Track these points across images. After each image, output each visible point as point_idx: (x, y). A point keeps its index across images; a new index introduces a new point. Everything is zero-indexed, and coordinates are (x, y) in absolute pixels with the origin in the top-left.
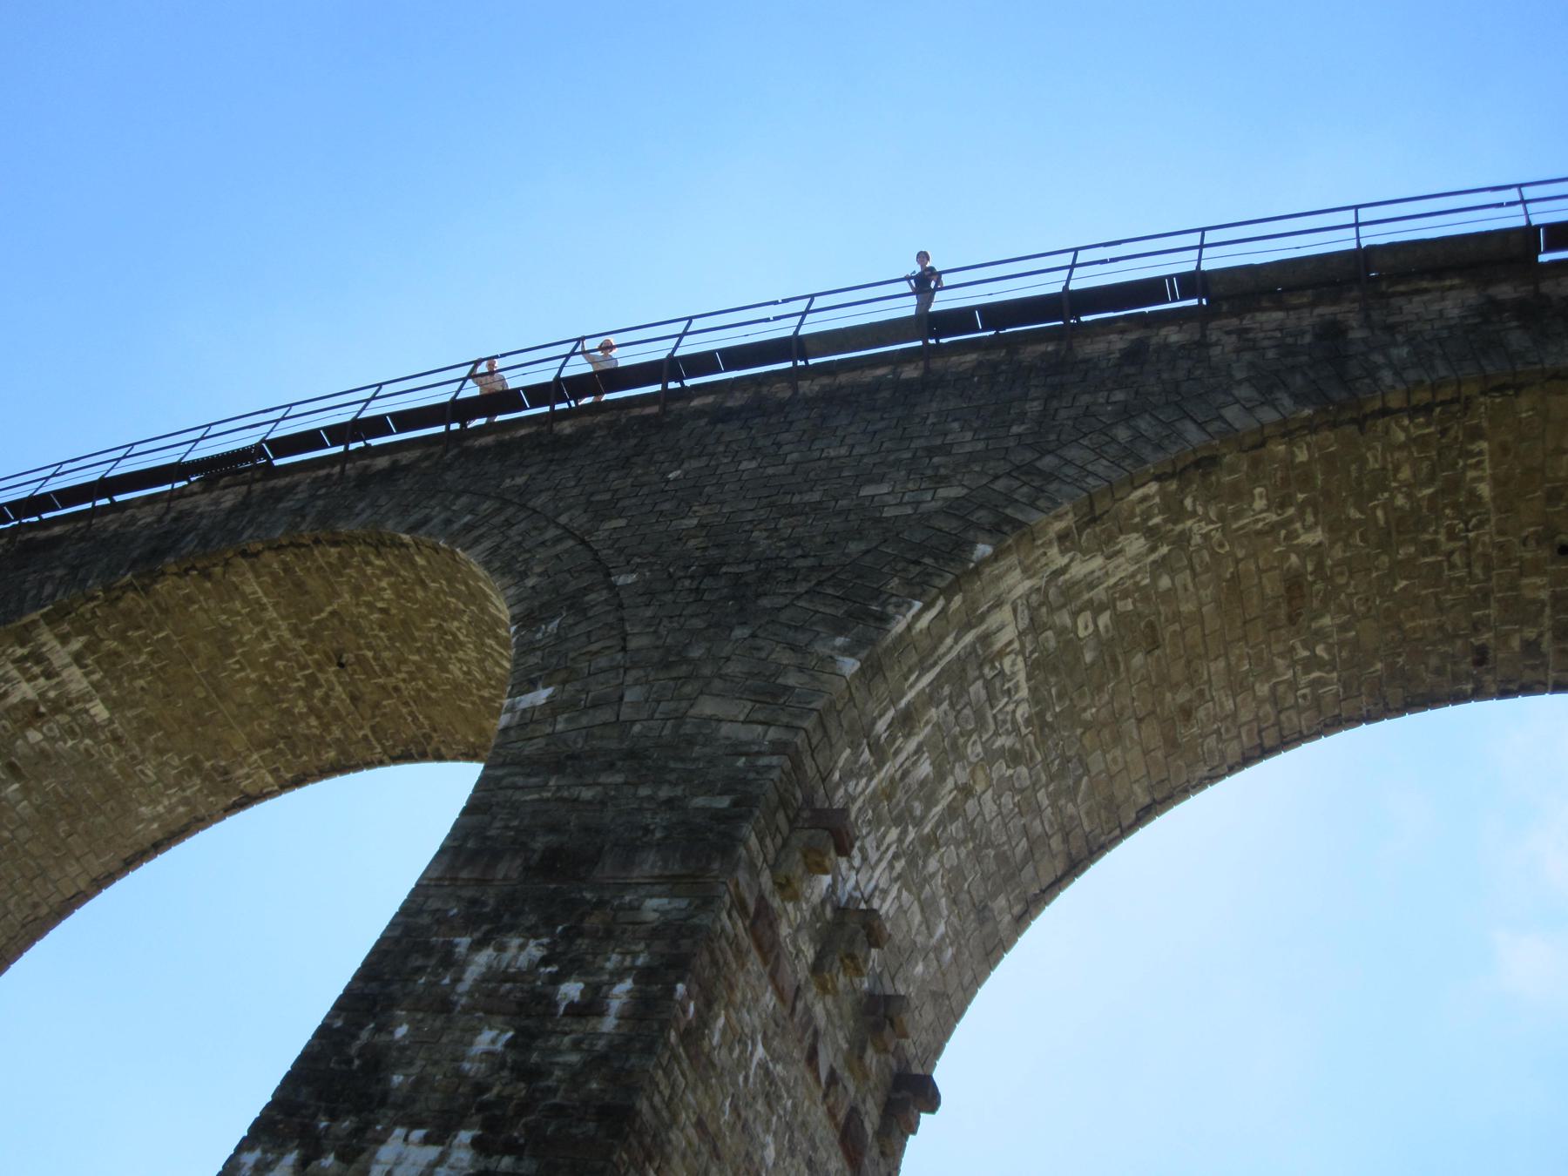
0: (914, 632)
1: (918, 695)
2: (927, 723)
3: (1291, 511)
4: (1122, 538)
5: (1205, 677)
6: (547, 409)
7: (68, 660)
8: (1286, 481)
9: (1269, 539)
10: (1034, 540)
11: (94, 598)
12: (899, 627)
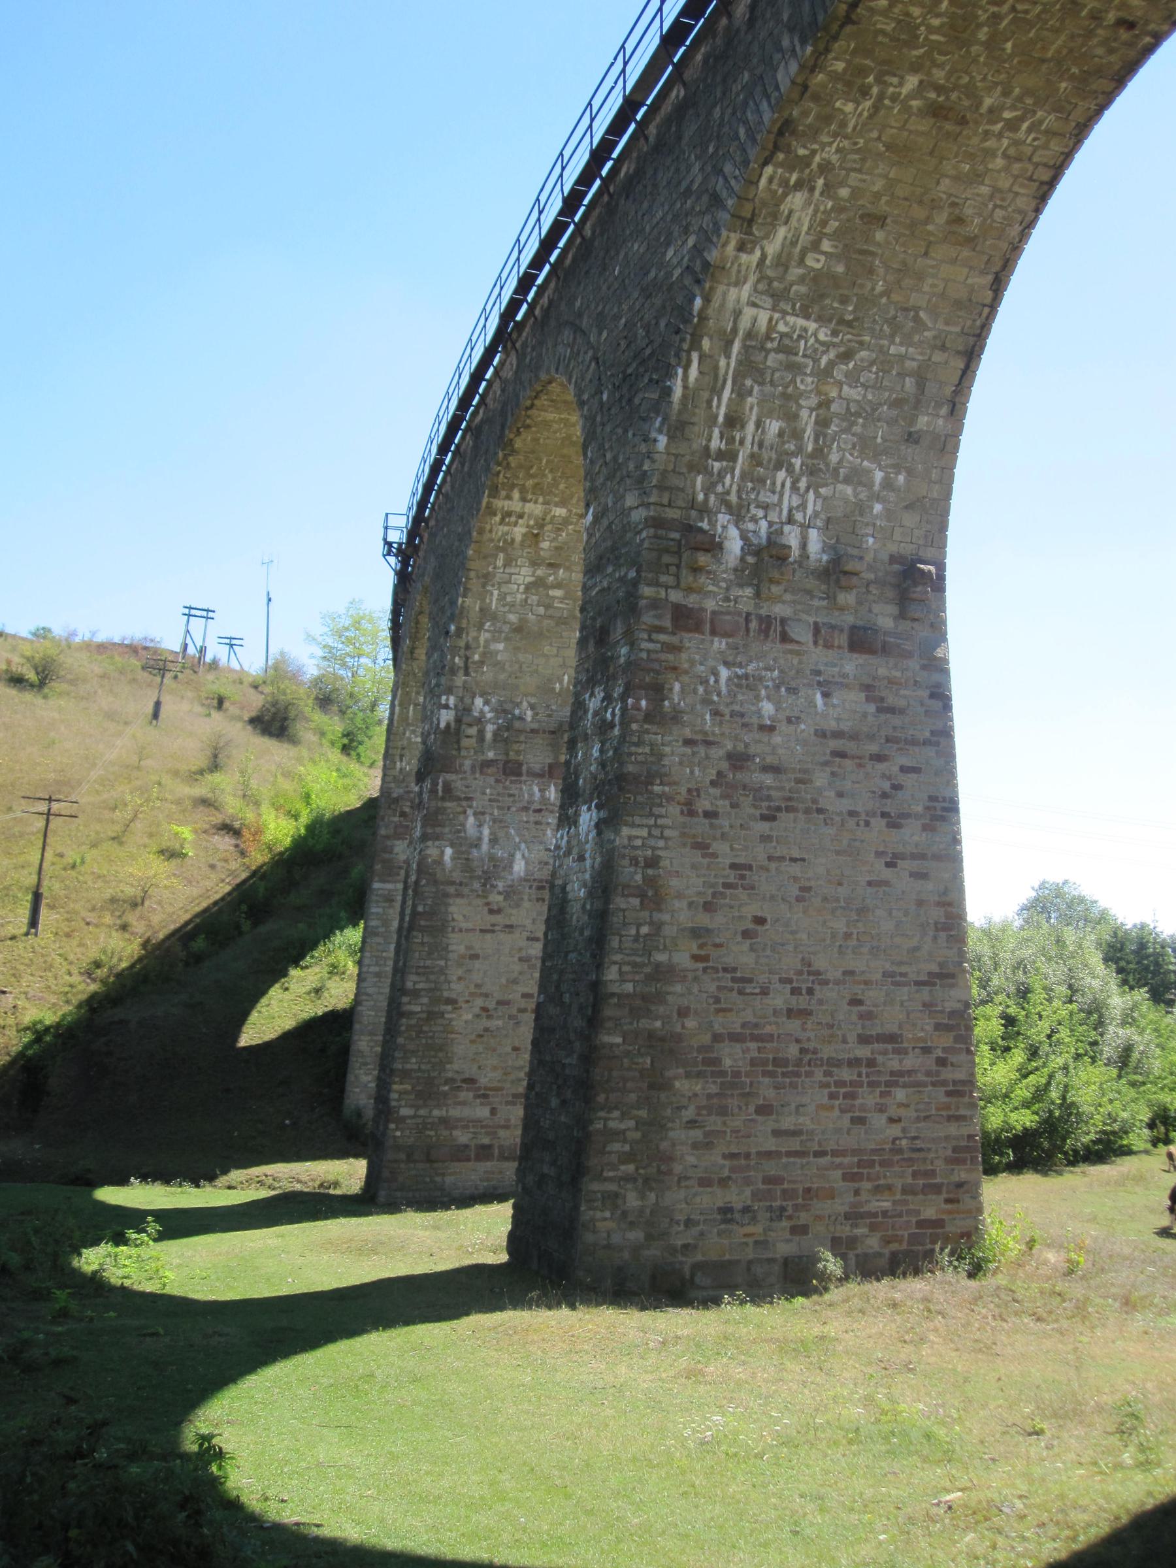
0: (691, 386)
1: (728, 406)
2: (751, 409)
3: (875, 90)
4: (782, 207)
5: (944, 196)
6: (633, 126)
7: (521, 504)
8: (849, 84)
9: (882, 112)
10: (723, 268)
11: (499, 473)
12: (678, 392)
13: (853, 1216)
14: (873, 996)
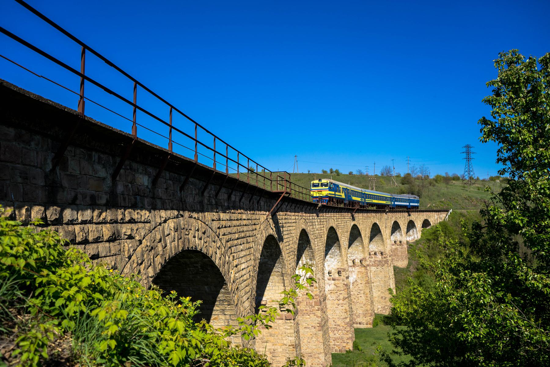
13: (334, 345)
14: (336, 320)
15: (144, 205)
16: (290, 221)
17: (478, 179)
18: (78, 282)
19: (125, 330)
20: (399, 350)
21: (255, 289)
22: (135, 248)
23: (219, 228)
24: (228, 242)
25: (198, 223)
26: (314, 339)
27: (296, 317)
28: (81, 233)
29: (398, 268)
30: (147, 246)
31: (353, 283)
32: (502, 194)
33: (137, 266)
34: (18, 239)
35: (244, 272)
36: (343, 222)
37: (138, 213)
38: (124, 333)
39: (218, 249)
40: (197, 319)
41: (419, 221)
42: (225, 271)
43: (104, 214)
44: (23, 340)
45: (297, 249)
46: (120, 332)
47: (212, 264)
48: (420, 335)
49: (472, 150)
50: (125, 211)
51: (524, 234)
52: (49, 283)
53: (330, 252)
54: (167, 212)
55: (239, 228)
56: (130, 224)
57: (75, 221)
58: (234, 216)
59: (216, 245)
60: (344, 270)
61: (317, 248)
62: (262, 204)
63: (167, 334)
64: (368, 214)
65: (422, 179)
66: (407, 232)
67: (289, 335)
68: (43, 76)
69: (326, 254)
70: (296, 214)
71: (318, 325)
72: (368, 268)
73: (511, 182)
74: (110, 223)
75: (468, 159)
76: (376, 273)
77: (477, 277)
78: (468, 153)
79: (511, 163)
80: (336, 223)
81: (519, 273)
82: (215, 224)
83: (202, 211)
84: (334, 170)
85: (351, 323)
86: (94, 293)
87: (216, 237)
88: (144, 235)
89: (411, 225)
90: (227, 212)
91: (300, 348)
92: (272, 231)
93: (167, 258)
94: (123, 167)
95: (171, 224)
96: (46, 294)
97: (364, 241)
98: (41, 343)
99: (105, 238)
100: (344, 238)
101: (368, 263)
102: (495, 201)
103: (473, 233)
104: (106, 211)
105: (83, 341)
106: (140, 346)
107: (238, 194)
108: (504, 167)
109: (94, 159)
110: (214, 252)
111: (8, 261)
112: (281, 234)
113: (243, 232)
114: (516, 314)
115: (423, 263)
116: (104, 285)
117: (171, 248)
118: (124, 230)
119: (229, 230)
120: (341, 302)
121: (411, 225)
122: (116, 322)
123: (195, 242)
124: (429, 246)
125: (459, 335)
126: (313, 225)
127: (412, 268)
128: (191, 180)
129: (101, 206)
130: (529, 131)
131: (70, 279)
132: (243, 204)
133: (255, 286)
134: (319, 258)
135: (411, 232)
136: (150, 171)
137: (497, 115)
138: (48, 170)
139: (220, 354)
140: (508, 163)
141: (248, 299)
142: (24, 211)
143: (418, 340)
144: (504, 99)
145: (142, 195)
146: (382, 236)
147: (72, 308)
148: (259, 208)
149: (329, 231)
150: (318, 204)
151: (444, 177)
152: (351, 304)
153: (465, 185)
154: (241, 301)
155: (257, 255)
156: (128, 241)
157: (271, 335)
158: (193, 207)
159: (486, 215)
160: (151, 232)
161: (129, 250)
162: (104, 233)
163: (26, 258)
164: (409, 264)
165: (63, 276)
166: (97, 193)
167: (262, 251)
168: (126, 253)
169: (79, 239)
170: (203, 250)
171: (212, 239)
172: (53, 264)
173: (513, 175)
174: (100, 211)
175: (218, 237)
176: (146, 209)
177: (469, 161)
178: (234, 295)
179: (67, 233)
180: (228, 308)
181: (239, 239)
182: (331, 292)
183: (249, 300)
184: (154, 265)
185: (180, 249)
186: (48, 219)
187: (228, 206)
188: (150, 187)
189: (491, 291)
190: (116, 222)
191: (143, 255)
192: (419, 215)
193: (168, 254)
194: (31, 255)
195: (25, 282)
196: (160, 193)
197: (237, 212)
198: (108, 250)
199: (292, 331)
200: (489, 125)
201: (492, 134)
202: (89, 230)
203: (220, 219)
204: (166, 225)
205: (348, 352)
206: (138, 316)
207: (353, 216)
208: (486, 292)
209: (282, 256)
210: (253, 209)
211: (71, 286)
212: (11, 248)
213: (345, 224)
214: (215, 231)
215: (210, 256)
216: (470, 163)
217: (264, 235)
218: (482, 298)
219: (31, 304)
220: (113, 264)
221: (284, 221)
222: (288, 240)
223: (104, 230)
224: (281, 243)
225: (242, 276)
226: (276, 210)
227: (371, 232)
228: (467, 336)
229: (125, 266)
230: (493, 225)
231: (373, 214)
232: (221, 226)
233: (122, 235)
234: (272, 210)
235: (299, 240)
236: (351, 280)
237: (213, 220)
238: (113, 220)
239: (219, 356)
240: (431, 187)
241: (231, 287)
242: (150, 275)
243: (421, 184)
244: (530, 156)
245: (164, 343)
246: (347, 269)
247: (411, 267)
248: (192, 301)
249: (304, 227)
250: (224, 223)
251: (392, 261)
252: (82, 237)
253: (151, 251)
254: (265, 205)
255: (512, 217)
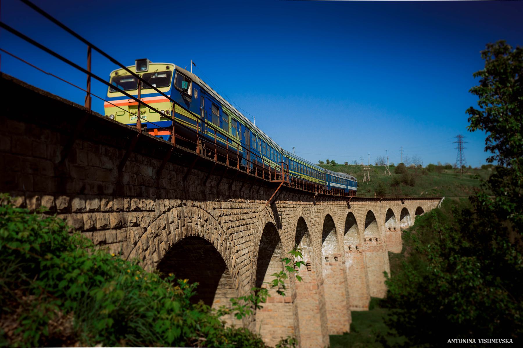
15: (149, 195)
16: (288, 209)
17: (470, 167)
18: (80, 266)
19: (122, 309)
20: (394, 331)
21: (255, 273)
22: (141, 235)
23: (220, 216)
24: (229, 229)
25: (200, 212)
26: (312, 321)
27: (295, 300)
28: (89, 221)
29: (393, 253)
30: (152, 233)
31: (349, 268)
32: (490, 181)
33: (142, 252)
34: (24, 226)
35: (244, 257)
36: (339, 210)
37: (143, 202)
38: (122, 312)
39: (219, 236)
40: (194, 300)
41: (412, 209)
42: (226, 257)
43: (111, 203)
44: (26, 318)
45: (295, 235)
46: (117, 311)
47: (214, 250)
48: (413, 317)
49: (464, 140)
50: (131, 200)
51: (512, 220)
52: (53, 266)
53: (327, 238)
54: (170, 201)
55: (239, 215)
56: (135, 213)
57: (84, 209)
58: (235, 205)
59: (218, 232)
60: (340, 255)
61: (314, 234)
62: (261, 193)
63: (164, 315)
64: (363, 202)
65: (415, 169)
66: (401, 219)
67: (288, 317)
68: (46, 75)
69: (323, 241)
70: (294, 202)
71: (316, 308)
72: (364, 253)
73: (499, 170)
74: (116, 212)
75: (460, 149)
76: (371, 258)
77: (467, 261)
78: (460, 143)
79: (499, 151)
80: (332, 211)
81: (508, 257)
82: (217, 213)
83: (204, 200)
84: (330, 161)
85: (348, 306)
86: (96, 276)
87: (218, 224)
88: (149, 223)
89: (405, 212)
90: (228, 200)
91: (299, 330)
92: (271, 219)
93: (171, 244)
94: (129, 159)
95: (175, 212)
96: (50, 276)
97: (359, 228)
98: (42, 322)
99: (112, 225)
100: (340, 224)
101: (363, 249)
102: (484, 188)
103: (463, 219)
104: (113, 200)
105: (84, 321)
106: (136, 325)
107: (239, 184)
108: (492, 155)
109: (100, 152)
110: (215, 239)
111: (13, 246)
112: (280, 221)
113: (243, 219)
114: (506, 297)
115: (418, 247)
116: (105, 268)
117: (175, 235)
118: (130, 218)
119: (230, 218)
120: (338, 285)
121: (405, 212)
122: (114, 302)
123: (198, 229)
124: (422, 233)
125: (449, 317)
126: (310, 213)
127: (406, 255)
128: (193, 171)
129: (108, 195)
130: (516, 120)
131: (73, 262)
132: (244, 194)
133: (255, 271)
134: (316, 244)
135: (405, 218)
136: (155, 162)
137: (483, 105)
138: (57, 162)
139: (215, 333)
140: (497, 151)
141: (248, 283)
142: (34, 201)
143: (412, 322)
144: (492, 88)
145: (147, 185)
146: (377, 223)
147: (74, 289)
148: (259, 197)
149: (325, 218)
150: (315, 194)
151: (436, 166)
152: (348, 288)
153: (458, 174)
154: (242, 285)
155: (256, 241)
156: (134, 228)
157: (271, 318)
158: (196, 196)
159: (475, 201)
160: (156, 220)
161: (135, 237)
162: (111, 221)
163: (31, 243)
164: (404, 250)
165: (66, 259)
166: (104, 183)
167: (262, 237)
168: (132, 239)
169: (86, 227)
170: (205, 236)
171: (214, 226)
172: (58, 249)
173: (501, 163)
174: (107, 200)
175: (220, 225)
176: (151, 198)
177: (461, 150)
178: (235, 279)
179: (75, 221)
180: (230, 291)
181: (240, 226)
182: (328, 276)
183: (250, 284)
184: (159, 251)
185: (184, 236)
186: (58, 208)
187: (229, 195)
188: (154, 177)
189: (480, 274)
190: (122, 210)
191: (148, 242)
192: (412, 203)
193: (172, 241)
194: (36, 239)
195: (30, 266)
196: (164, 184)
197: (237, 201)
198: (115, 237)
199: (291, 313)
200: (477, 114)
201: (479, 124)
202: (96, 218)
203: (221, 207)
204: (170, 213)
205: (345, 334)
206: (135, 297)
207: (348, 204)
208: (476, 275)
209: (281, 243)
210: (253, 198)
211: (74, 269)
212: (17, 233)
213: (341, 212)
214: (217, 219)
215: (212, 242)
216: (462, 153)
217: (264, 223)
218: (471, 281)
219: (35, 286)
220: (120, 249)
221: (282, 209)
222: (287, 227)
223: (111, 218)
224: (279, 230)
225: (242, 261)
226: (275, 199)
227: (366, 219)
228: (458, 318)
229: (131, 252)
230: (483, 211)
231: (368, 202)
232: (222, 214)
233: (129, 223)
234: (271, 199)
235: (297, 227)
236: (348, 264)
237: (215, 209)
238: (120, 209)
239: (215, 335)
240: (424, 176)
241: (232, 271)
242: (155, 260)
243: (414, 173)
244: (518, 143)
245: (160, 322)
246: (343, 254)
247: (406, 253)
248: (189, 283)
249: (301, 215)
250: (225, 211)
251: (386, 247)
252: (89, 225)
253: (156, 237)
254: (265, 194)
255: (500, 203)
